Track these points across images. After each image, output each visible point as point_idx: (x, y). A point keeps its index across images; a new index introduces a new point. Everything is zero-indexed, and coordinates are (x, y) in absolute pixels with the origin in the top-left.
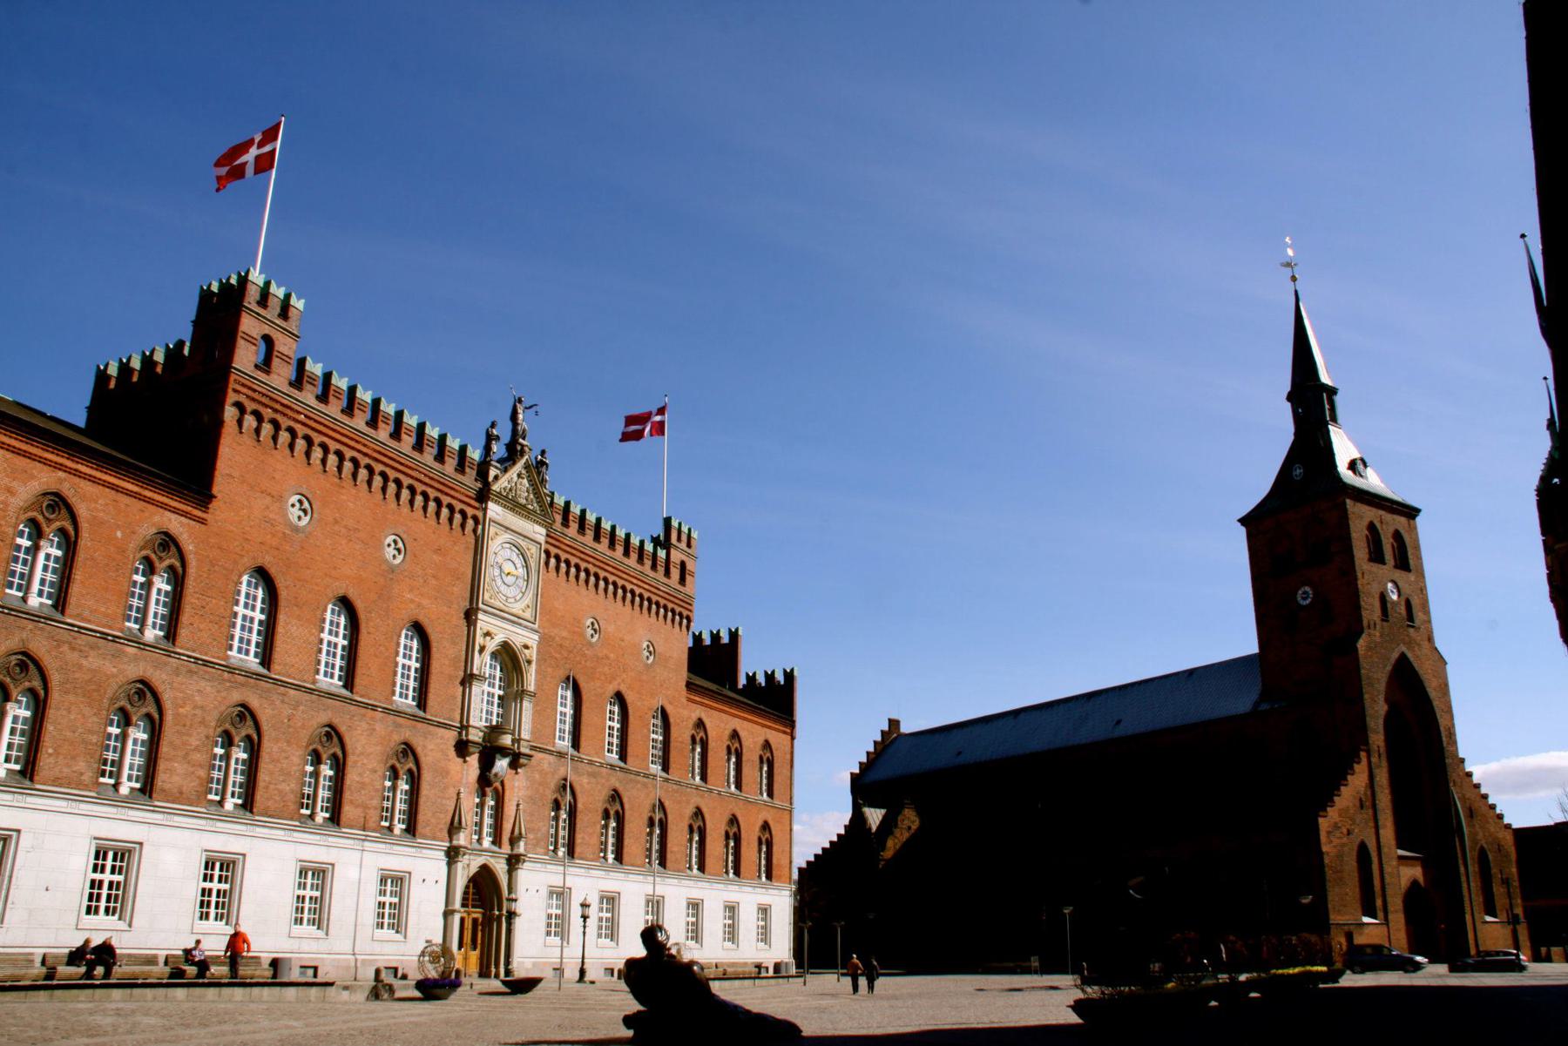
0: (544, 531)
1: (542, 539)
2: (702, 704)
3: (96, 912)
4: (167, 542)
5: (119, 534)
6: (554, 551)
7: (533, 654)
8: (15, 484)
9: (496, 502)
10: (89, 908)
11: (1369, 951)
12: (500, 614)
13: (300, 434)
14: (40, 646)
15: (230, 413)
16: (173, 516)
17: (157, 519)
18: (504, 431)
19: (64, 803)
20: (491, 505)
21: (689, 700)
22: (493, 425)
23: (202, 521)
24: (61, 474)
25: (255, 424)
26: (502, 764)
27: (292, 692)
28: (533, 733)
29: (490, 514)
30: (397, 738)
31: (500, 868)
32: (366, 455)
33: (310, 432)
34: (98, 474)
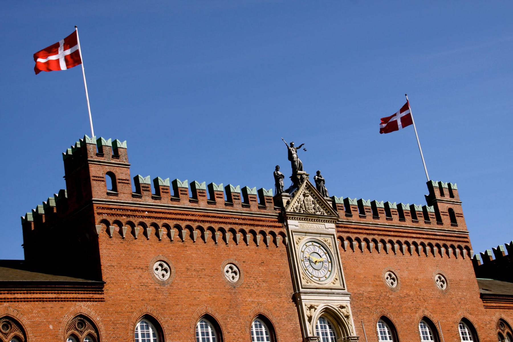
1: (334, 231)
2: (500, 308)
5: (51, 327)
12: (317, 291)
15: (100, 228)
17: (72, 309)
18: (286, 171)
20: (290, 222)
21: (487, 307)
22: (277, 168)
23: (102, 300)
25: (118, 229)
29: (290, 228)
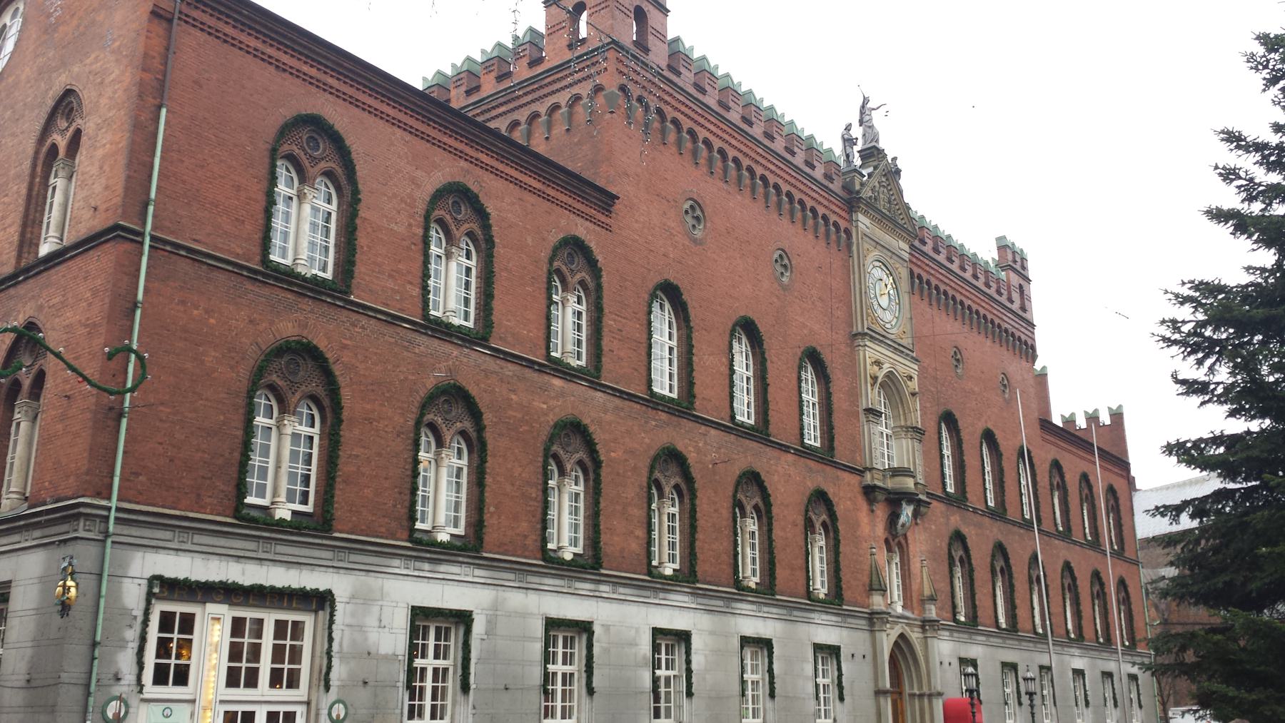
0: (906, 247)
3: (420, 716)
4: (575, 246)
6: (917, 271)
7: (914, 385)
8: (419, 173)
9: (866, 213)
10: (412, 708)
11: (35, 230)
13: (771, 182)
14: (325, 328)
16: (579, 221)
19: (328, 554)
23: (608, 228)
24: (462, 163)
26: (907, 511)
27: (713, 432)
28: (926, 478)
30: (811, 485)
31: (915, 636)
32: (746, 155)
33: (726, 147)
34: (501, 167)
